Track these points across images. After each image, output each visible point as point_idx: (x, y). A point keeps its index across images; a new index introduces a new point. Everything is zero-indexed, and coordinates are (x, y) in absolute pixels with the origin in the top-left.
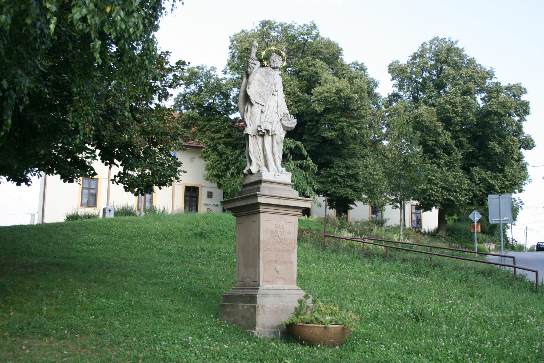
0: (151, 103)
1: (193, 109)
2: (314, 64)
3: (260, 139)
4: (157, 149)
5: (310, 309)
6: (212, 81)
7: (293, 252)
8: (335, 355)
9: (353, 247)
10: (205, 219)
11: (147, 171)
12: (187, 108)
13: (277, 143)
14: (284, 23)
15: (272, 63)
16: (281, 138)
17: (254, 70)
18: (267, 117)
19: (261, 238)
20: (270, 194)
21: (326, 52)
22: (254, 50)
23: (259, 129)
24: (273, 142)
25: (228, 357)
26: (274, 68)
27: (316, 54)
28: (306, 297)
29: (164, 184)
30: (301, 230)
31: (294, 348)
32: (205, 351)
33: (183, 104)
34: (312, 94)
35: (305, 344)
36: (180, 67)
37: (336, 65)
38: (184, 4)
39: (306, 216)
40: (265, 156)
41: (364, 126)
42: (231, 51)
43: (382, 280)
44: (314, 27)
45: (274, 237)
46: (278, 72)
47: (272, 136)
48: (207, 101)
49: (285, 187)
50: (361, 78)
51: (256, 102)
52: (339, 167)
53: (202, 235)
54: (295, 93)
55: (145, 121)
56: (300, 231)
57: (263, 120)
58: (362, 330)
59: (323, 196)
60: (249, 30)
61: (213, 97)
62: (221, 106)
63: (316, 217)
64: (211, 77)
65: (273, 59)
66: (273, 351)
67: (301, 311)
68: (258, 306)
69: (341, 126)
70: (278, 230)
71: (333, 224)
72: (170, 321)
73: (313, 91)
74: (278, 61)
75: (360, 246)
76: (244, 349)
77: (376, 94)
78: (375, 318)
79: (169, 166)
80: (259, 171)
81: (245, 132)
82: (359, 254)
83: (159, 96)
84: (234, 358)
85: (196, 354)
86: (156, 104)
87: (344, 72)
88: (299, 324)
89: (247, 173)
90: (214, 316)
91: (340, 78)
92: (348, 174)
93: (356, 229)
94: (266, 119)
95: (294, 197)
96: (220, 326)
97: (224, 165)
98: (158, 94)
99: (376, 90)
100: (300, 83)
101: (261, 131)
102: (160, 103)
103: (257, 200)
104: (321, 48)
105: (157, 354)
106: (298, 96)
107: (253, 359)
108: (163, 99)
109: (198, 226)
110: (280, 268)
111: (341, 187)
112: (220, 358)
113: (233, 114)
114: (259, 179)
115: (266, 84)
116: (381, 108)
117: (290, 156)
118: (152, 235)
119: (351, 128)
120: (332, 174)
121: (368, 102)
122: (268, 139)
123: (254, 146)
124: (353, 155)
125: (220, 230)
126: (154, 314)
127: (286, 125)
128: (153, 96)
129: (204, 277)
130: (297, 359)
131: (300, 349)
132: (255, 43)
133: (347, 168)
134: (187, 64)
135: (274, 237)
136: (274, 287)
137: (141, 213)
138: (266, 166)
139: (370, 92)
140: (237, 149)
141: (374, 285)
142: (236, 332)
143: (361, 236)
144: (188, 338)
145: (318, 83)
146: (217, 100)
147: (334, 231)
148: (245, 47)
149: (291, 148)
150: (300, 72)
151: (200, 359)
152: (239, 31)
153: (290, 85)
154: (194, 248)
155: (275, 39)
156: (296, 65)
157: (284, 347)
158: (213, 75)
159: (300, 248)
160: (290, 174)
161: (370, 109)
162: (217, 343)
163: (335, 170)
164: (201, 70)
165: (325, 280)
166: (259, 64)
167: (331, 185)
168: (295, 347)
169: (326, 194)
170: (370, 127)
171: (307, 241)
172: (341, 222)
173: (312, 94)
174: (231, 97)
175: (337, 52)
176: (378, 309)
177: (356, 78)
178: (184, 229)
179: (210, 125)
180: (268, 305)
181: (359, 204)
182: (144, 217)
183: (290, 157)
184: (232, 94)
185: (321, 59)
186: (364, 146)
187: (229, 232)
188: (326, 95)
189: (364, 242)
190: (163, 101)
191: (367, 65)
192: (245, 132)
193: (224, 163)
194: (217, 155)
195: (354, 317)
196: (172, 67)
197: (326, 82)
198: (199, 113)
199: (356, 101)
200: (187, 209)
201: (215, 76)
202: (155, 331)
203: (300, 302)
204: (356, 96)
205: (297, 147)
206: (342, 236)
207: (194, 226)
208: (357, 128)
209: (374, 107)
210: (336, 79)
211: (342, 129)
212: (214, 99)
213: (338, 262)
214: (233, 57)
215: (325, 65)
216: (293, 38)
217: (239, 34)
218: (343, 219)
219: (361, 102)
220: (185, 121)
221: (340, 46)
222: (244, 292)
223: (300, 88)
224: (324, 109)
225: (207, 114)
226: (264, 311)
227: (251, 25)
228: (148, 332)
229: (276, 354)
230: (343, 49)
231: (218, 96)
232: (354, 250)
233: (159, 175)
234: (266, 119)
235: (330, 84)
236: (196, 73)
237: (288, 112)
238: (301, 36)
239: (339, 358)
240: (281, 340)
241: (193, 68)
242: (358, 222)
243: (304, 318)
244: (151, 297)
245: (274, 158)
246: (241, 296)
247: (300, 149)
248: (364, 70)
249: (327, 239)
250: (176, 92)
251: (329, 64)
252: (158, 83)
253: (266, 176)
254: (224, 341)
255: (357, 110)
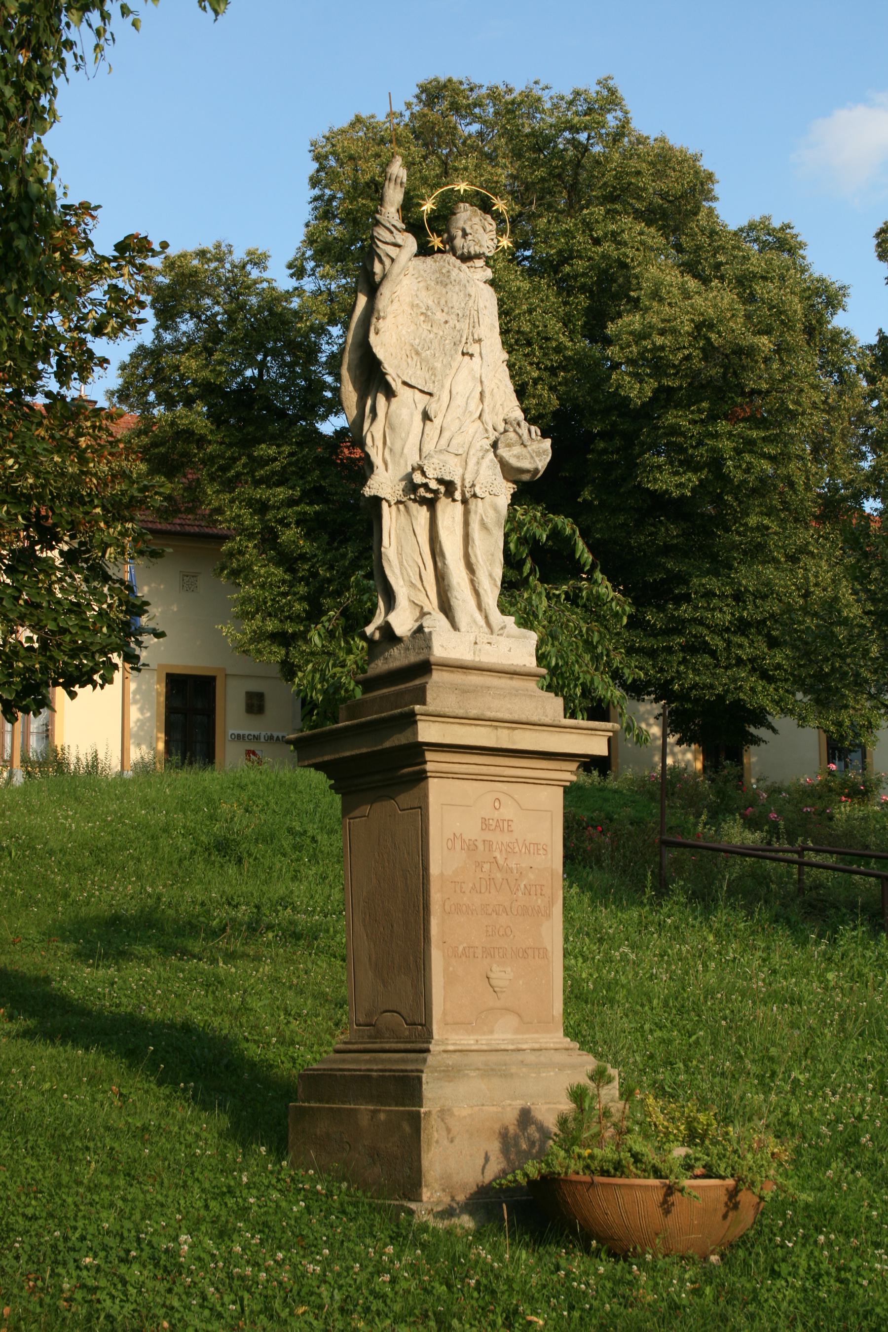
0: (33, 392)
1: (189, 402)
2: (614, 234)
3: (422, 514)
4: (56, 553)
5: (614, 1119)
6: (254, 300)
7: (549, 916)
8: (708, 1290)
9: (763, 880)
10: (237, 792)
11: (24, 633)
12: (167, 399)
13: (484, 525)
14: (502, 88)
15: (459, 242)
16: (496, 510)
17: (397, 269)
18: (446, 435)
19: (434, 870)
20: (461, 712)
21: (651, 186)
22: (394, 196)
23: (418, 478)
24: (466, 524)
25: (321, 1307)
26: (466, 258)
27: (617, 196)
28: (599, 1076)
29: (85, 679)
30: (579, 823)
31: (558, 1268)
32: (232, 1282)
33: (152, 386)
34: (608, 341)
35: (598, 1251)
36: (131, 262)
37: (693, 236)
38: (143, 26)
39: (595, 773)
40: (441, 577)
41: (794, 449)
42: (317, 192)
43: (871, 1004)
44: (611, 99)
45: (479, 865)
46: (481, 273)
47: (465, 502)
48: (239, 372)
49: (517, 683)
50: (782, 278)
51: (405, 383)
52: (709, 595)
53: (224, 848)
54: (547, 339)
55: (12, 454)
56: (573, 828)
57: (429, 447)
58: (804, 1196)
59: (657, 700)
60: (381, 117)
61: (260, 357)
62: (285, 388)
63: (629, 773)
64: (249, 287)
65: (461, 224)
66: (484, 1281)
67: (580, 1129)
68: (428, 1114)
69: (713, 450)
70: (493, 833)
71: (693, 801)
72: (113, 1172)
73: (611, 329)
74: (479, 232)
75: (790, 874)
76: (379, 1273)
77: (836, 334)
78: (849, 1145)
79: (101, 613)
80: (420, 629)
81: (368, 492)
82: (784, 906)
83: (59, 364)
84: (342, 1310)
85: (204, 1298)
86: (48, 394)
87: (721, 258)
88: (575, 1178)
89: (377, 636)
90: (269, 1151)
91: (705, 281)
92: (741, 619)
93: (773, 816)
94: (443, 442)
95: (548, 720)
96: (292, 1190)
97: (302, 599)
98: (54, 360)
99: (839, 321)
100: (565, 303)
101: (426, 486)
102: (64, 391)
103: (415, 733)
104: (638, 173)
105: (63, 1304)
106: (559, 350)
107: (411, 1314)
108: (75, 375)
109: (212, 818)
110: (502, 975)
111: (717, 666)
112: (291, 1313)
113: (332, 418)
114: (421, 657)
115: (440, 316)
116: (854, 385)
117: (532, 567)
118: (51, 853)
119: (747, 457)
120: (684, 621)
121: (805, 362)
122: (450, 514)
123: (401, 541)
124: (757, 552)
125: (290, 830)
126: (55, 1150)
127: (514, 462)
128: (40, 366)
129: (237, 1005)
130: (571, 1308)
131: (586, 1272)
132: (398, 169)
133: (738, 597)
134: (156, 247)
135: (479, 865)
136: (483, 1040)
137: (11, 775)
138: (446, 608)
139: (814, 329)
140: (345, 541)
141: (843, 1020)
142: (350, 1209)
143: (791, 837)
144: (175, 1239)
145: (630, 299)
146: (274, 371)
147: (696, 825)
148: (368, 177)
149: (536, 541)
150: (565, 261)
151: (220, 1316)
152: (343, 122)
153: (530, 311)
154: (200, 898)
155: (469, 146)
156: (547, 236)
157: (521, 1262)
158: (255, 282)
159: (575, 890)
160: (533, 637)
161: (815, 387)
162: (280, 1255)
163: (696, 608)
164: (213, 265)
165: (666, 1004)
166: (410, 243)
167: (684, 661)
168: (563, 1263)
169: (663, 692)
170: (815, 450)
171: (598, 861)
172: (720, 793)
173: (608, 341)
174: (323, 358)
175: (693, 189)
176: (858, 1109)
177: (764, 278)
178: (165, 830)
179: (250, 457)
180: (462, 1111)
181: (783, 722)
182: (24, 791)
183: (532, 571)
184: (325, 347)
185: (638, 215)
186: (796, 520)
187: (322, 838)
188: (659, 341)
189: (802, 864)
190: (73, 384)
191: (802, 231)
192: (368, 492)
193: (302, 589)
194: (278, 564)
195: (773, 1145)
196: (104, 259)
197: (656, 295)
198: (209, 415)
199: (766, 360)
200: (176, 758)
201: (265, 285)
202: (59, 1213)
203: (578, 1095)
204: (765, 342)
205: (555, 534)
206: (723, 843)
207: (199, 817)
208: (772, 459)
209: (828, 382)
210: (692, 284)
211: (716, 463)
212: (262, 366)
213: (711, 938)
214: (326, 215)
215: (654, 236)
216: (541, 142)
217: (343, 132)
218: (725, 782)
219: (783, 363)
220: (162, 444)
221: (706, 164)
222: (375, 1061)
223: (567, 321)
224: (656, 392)
225: (239, 420)
226: (449, 1130)
227: (387, 95)
228: (34, 1218)
229: (493, 1292)
230: (717, 176)
231: (276, 353)
232: (769, 891)
233: (66, 647)
234: (443, 442)
235: (672, 301)
236: (195, 273)
237: (519, 415)
238: (567, 134)
239: (722, 1301)
240: (512, 1236)
241: (183, 256)
242: (778, 791)
243: (591, 1157)
244: (47, 1086)
245: (472, 582)
246: (365, 1078)
247: (568, 542)
248: (792, 251)
249: (671, 854)
250: (116, 350)
251: (665, 230)
252: (56, 319)
253: (446, 645)
254: (309, 1248)
255: (768, 392)
